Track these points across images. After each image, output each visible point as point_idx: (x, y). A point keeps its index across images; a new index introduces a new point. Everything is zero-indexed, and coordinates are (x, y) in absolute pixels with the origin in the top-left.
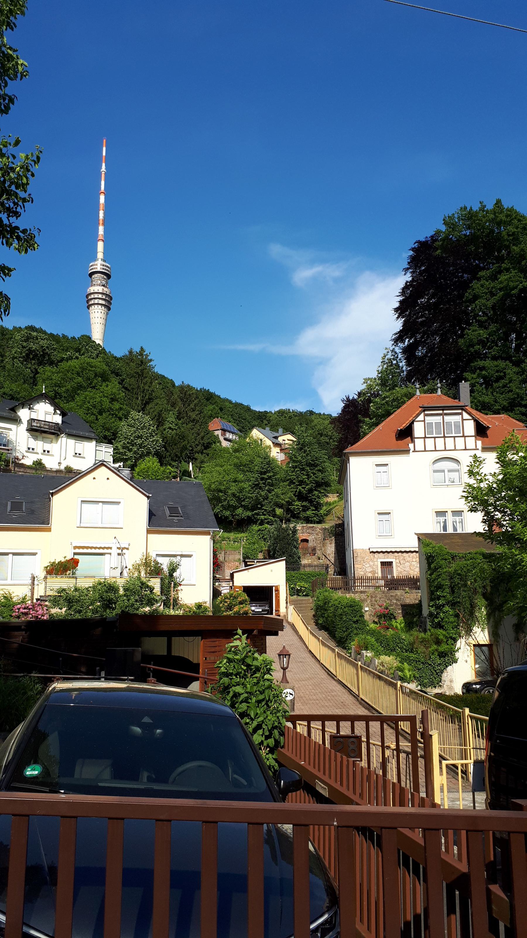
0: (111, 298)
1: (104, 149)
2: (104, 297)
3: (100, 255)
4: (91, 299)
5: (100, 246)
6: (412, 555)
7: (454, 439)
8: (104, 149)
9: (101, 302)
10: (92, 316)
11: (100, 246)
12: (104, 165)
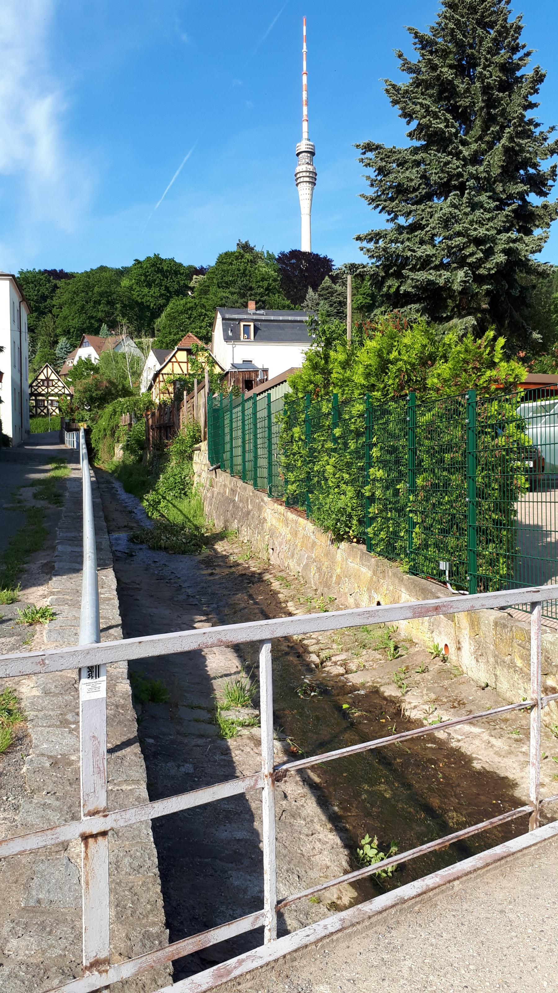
1: (305, 28)
2: (308, 174)
3: (305, 135)
5: (305, 125)
6: (25, 662)
7: (260, 467)
8: (305, 28)
9: (308, 179)
10: (300, 193)
11: (305, 125)
12: (305, 44)
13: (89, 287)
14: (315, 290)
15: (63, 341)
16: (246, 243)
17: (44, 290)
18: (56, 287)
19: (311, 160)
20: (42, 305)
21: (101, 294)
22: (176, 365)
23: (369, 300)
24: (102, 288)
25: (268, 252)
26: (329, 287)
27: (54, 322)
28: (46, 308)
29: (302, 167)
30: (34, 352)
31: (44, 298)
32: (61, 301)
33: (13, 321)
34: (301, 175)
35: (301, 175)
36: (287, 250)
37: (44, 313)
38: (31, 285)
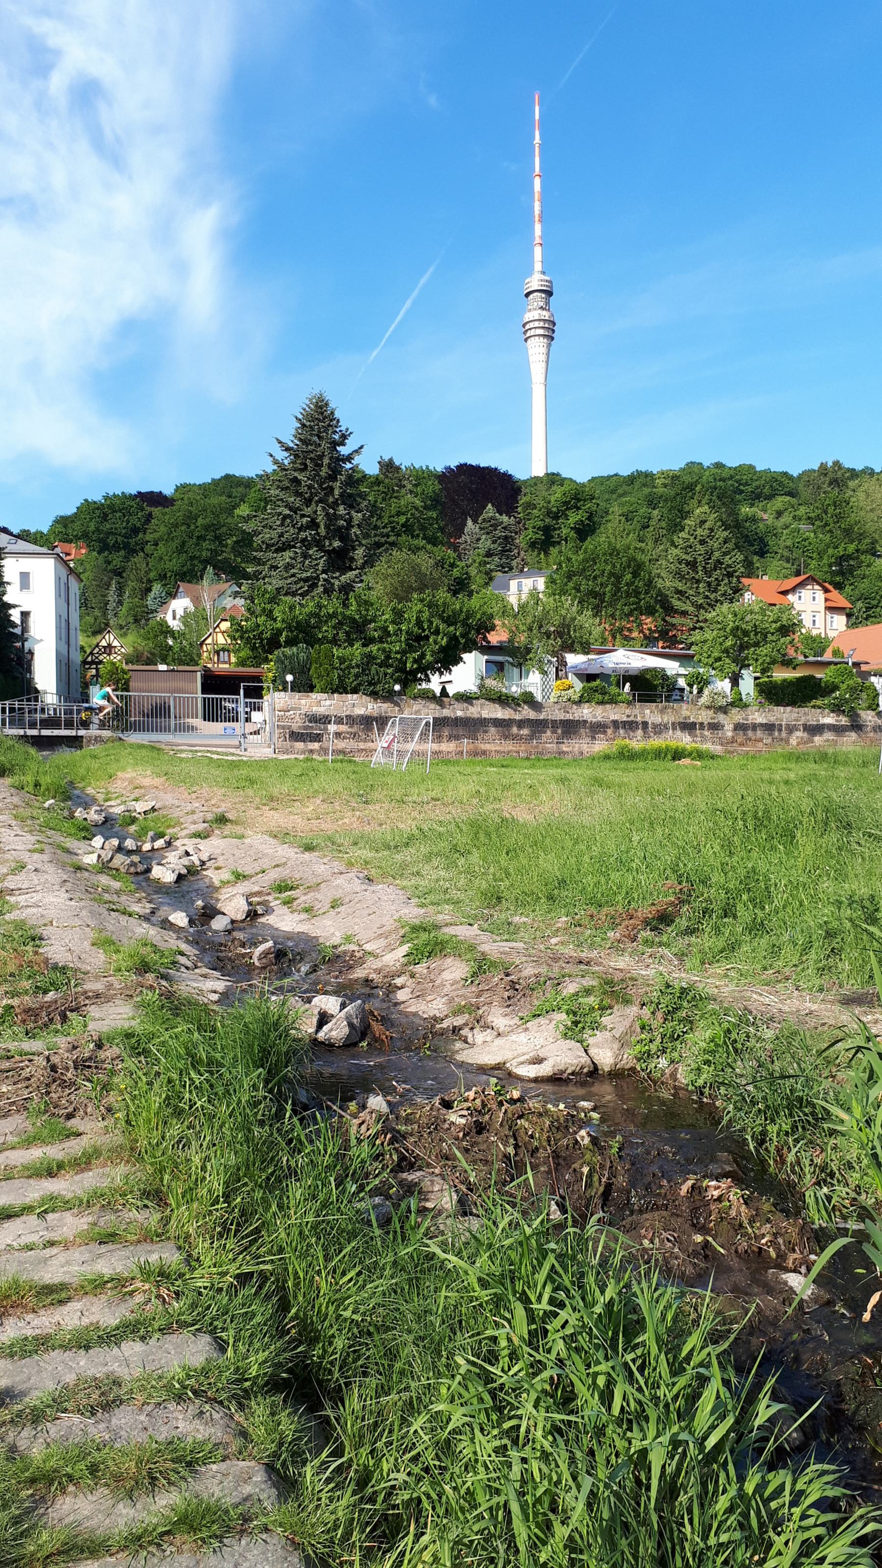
0: (554, 324)
2: (542, 324)
5: (538, 251)
9: (541, 332)
12: (537, 133)
13: (190, 518)
14: (475, 521)
15: (157, 588)
16: (391, 460)
17: (134, 521)
19: (547, 303)
20: (132, 541)
21: (206, 528)
23: (540, 536)
24: (208, 520)
25: (427, 467)
26: (492, 518)
27: (147, 564)
28: (137, 544)
29: (534, 313)
30: (120, 603)
31: (135, 531)
32: (157, 535)
33: (58, 595)
34: (531, 325)
35: (531, 325)
36: (453, 464)
37: (135, 551)
38: (119, 514)
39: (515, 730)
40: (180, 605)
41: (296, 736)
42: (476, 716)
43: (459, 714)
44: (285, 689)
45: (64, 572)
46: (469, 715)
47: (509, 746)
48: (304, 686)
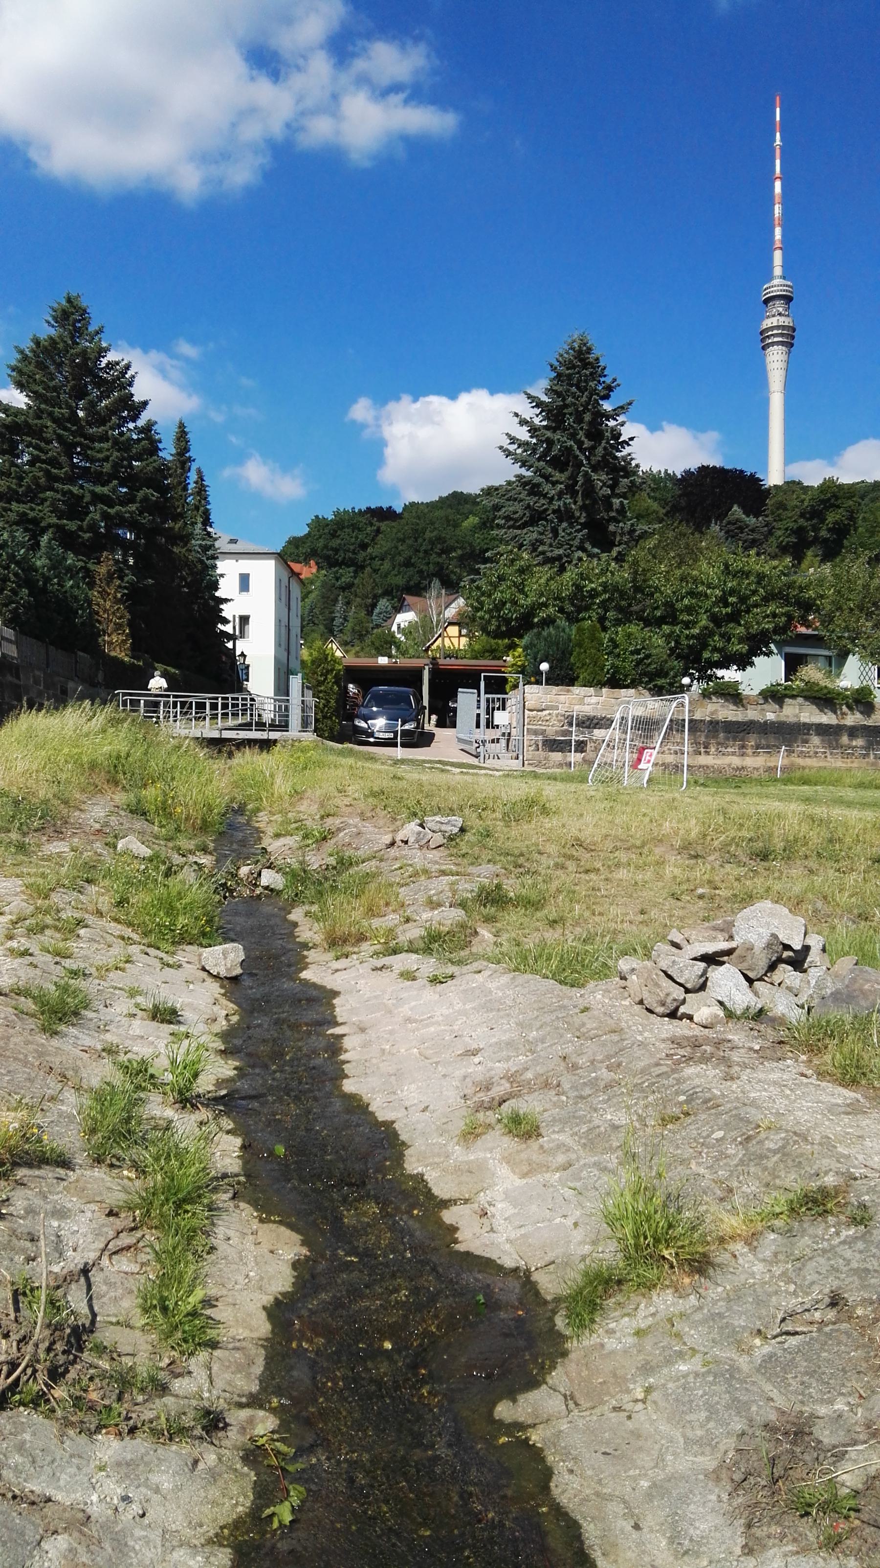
3: (778, 271)
4: (768, 337)
5: (778, 256)
10: (769, 359)
11: (778, 256)
12: (778, 135)
13: (417, 534)
18: (378, 531)
22: (447, 640)
25: (666, 471)
33: (278, 598)
39: (845, 739)
40: (405, 618)
41: (553, 745)
42: (792, 720)
43: (770, 716)
44: (538, 682)
45: (285, 575)
46: (783, 719)
47: (836, 762)
48: (563, 677)
